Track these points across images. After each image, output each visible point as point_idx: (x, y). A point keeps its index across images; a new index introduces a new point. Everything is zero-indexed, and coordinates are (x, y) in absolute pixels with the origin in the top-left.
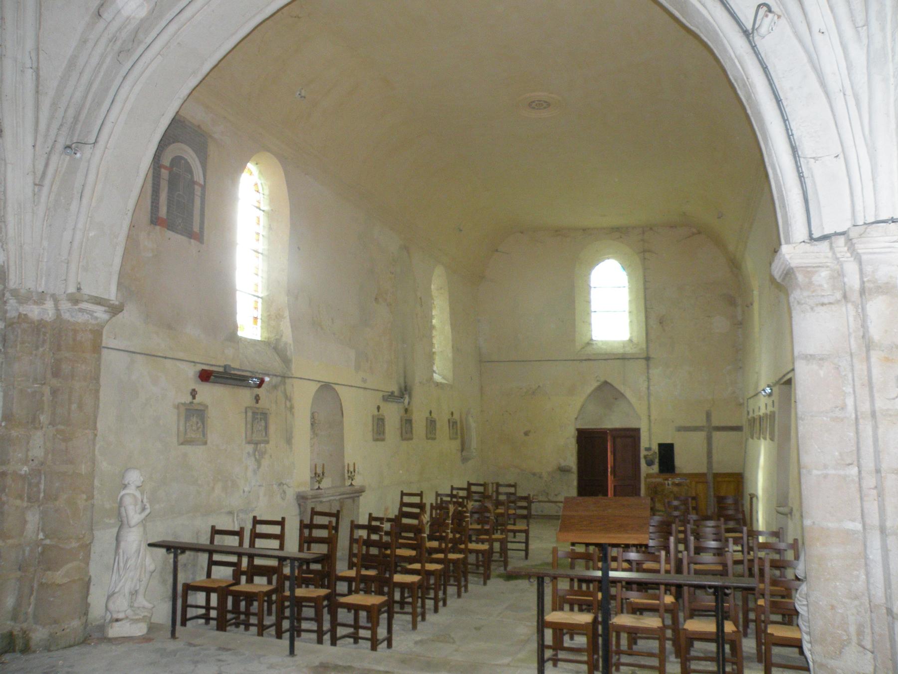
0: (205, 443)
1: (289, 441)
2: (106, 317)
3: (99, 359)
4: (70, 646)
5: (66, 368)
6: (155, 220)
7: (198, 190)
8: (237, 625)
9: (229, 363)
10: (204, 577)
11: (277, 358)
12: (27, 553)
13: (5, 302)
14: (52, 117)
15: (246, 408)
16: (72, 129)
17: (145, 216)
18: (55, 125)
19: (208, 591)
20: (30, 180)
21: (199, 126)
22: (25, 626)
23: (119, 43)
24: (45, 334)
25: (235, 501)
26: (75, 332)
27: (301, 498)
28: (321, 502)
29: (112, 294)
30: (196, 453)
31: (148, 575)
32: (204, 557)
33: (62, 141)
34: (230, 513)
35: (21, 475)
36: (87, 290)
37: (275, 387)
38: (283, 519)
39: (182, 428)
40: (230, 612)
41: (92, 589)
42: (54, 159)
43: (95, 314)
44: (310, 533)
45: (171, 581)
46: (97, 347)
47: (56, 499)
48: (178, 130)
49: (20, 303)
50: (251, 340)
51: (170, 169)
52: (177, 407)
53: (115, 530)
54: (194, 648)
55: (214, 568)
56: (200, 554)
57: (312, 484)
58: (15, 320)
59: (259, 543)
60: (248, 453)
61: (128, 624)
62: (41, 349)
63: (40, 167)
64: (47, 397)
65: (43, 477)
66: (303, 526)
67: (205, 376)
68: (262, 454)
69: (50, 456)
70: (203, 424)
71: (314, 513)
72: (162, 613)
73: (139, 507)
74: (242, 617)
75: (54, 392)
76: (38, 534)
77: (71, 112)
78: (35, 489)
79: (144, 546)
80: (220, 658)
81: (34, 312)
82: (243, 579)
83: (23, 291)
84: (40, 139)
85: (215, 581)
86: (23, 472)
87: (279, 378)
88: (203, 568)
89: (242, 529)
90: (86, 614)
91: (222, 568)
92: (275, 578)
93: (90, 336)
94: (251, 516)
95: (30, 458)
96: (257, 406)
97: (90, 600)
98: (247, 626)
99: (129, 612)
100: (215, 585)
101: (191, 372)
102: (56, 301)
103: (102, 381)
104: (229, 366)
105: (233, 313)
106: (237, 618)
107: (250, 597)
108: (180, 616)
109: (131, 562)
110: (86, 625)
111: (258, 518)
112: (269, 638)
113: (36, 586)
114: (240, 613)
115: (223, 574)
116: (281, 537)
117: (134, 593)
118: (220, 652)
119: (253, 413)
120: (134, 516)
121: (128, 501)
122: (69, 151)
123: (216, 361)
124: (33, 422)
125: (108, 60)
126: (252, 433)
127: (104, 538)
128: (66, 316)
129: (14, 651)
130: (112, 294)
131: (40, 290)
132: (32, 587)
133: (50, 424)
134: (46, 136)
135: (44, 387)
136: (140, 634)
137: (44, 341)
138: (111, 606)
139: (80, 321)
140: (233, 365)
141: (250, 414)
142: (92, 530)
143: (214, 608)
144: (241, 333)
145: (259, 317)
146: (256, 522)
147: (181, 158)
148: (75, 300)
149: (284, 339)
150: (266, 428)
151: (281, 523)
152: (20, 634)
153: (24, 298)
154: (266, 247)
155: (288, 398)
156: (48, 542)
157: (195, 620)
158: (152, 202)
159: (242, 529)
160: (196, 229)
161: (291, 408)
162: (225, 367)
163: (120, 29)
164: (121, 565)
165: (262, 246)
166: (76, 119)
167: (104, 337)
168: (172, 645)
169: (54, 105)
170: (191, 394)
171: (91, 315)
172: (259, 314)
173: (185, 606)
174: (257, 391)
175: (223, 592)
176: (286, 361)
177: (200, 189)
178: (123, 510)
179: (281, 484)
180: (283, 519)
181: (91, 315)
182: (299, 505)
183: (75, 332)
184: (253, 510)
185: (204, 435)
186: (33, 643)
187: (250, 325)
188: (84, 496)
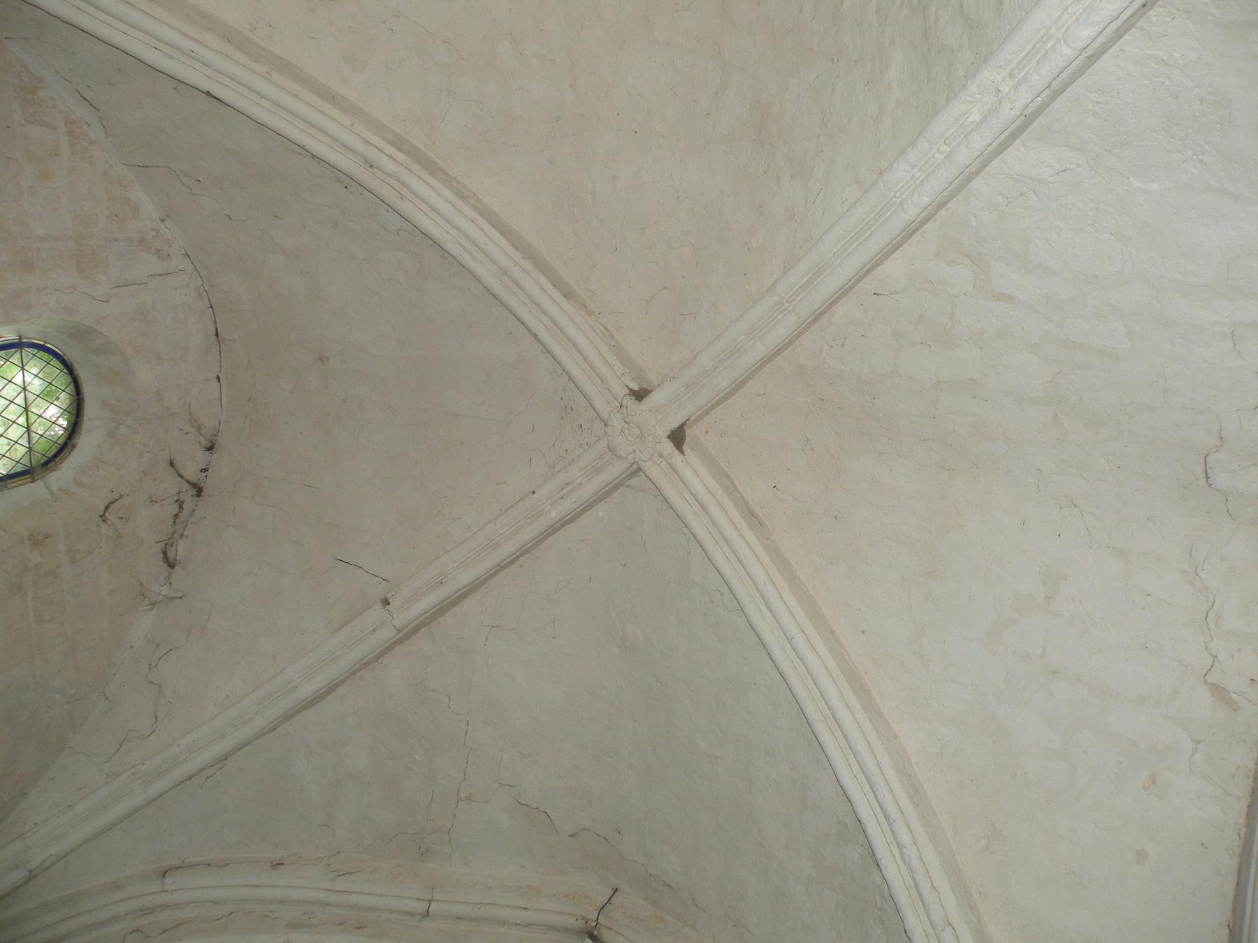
163: (165, 907)
182: (986, 60)
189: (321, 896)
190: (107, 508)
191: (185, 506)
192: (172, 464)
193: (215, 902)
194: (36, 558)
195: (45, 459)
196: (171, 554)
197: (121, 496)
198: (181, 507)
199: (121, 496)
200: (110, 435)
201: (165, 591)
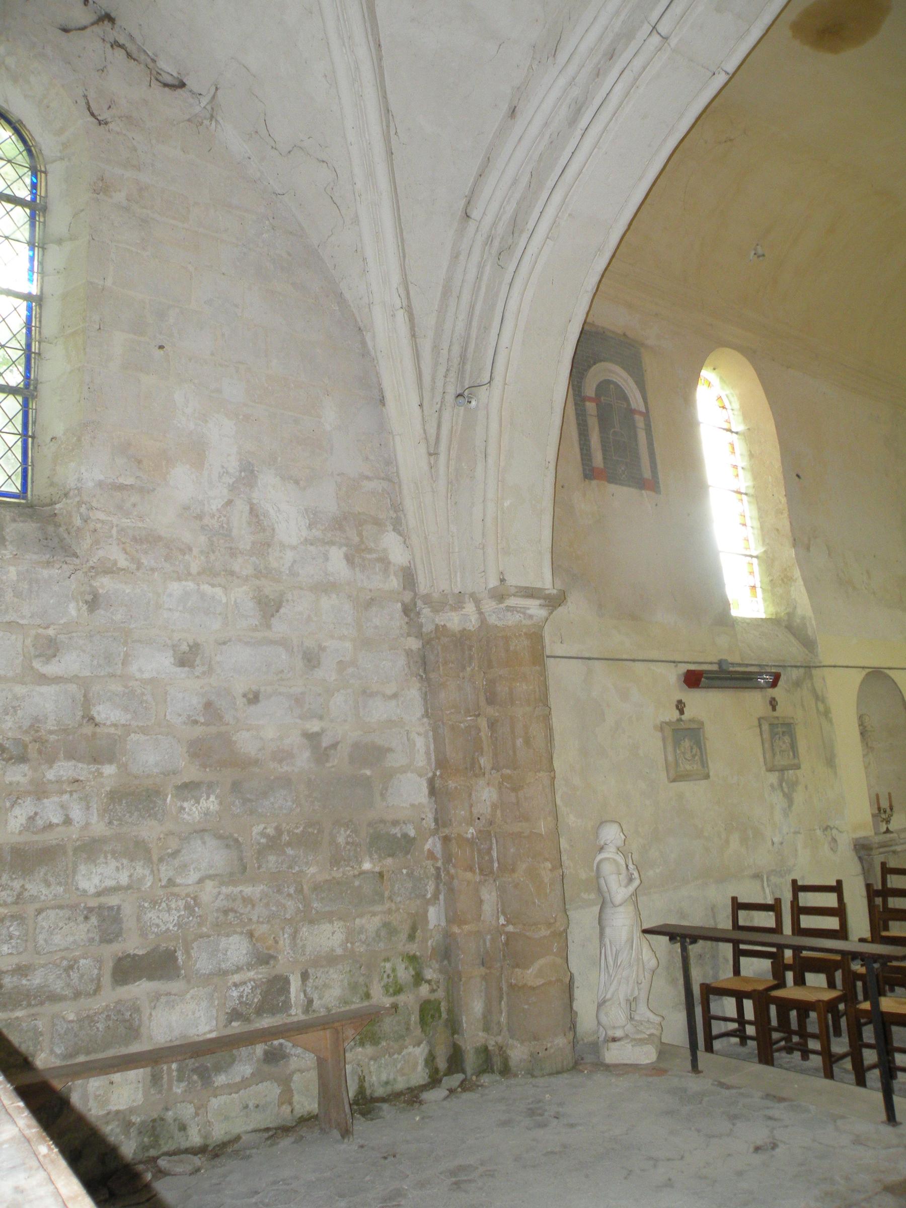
0: (707, 777)
1: (830, 761)
2: (543, 613)
3: (543, 673)
4: (558, 1073)
5: (502, 689)
6: (590, 473)
7: (640, 421)
8: (789, 1050)
9: (724, 657)
10: (730, 974)
11: (792, 639)
12: (488, 944)
13: (419, 613)
14: (436, 364)
15: (759, 719)
16: (461, 372)
17: (574, 469)
18: (442, 370)
19: (739, 995)
20: (423, 450)
21: (624, 335)
22: (500, 1039)
23: (496, 243)
24: (470, 649)
25: (762, 858)
26: (507, 639)
27: (862, 849)
28: (894, 852)
29: (546, 581)
30: (695, 793)
31: (648, 975)
32: (727, 949)
33: (452, 391)
34: (757, 876)
35: (468, 840)
36: (513, 581)
37: (798, 684)
38: (839, 882)
39: (671, 758)
40: (776, 1030)
41: (577, 993)
42: (446, 415)
43: (529, 612)
44: (885, 902)
45: (681, 981)
46: (538, 656)
47: (513, 871)
48: (592, 346)
49: (436, 611)
50: (751, 619)
51: (597, 399)
52: (661, 728)
53: (597, 909)
54: (727, 1093)
55: (743, 960)
56: (721, 944)
57: (876, 826)
58: (433, 635)
59: (807, 922)
60: (772, 786)
61: (629, 1046)
62: (468, 669)
63: (432, 431)
64: (485, 732)
65: (494, 841)
66: (871, 893)
67: (693, 680)
68: (793, 785)
69: (498, 812)
70: (700, 748)
71: (886, 870)
72: (676, 1029)
73: (623, 877)
74: (796, 1039)
75: (492, 725)
76: (498, 918)
77: (456, 349)
78: (487, 858)
79: (637, 933)
80: (770, 1113)
81: (453, 621)
82: (790, 976)
83: (436, 595)
84: (427, 395)
85: (747, 980)
86: (469, 836)
87: (802, 670)
88: (727, 960)
89: (778, 901)
90: (573, 1026)
91: (755, 960)
92: (838, 975)
93: (526, 643)
94: (789, 879)
95: (476, 816)
96: (775, 714)
97: (575, 1006)
98: (806, 1054)
99: (629, 1028)
100: (748, 988)
101: (672, 676)
102: (477, 602)
103: (552, 702)
104: (726, 661)
105: (719, 584)
106: (788, 1039)
107: (804, 1008)
108: (701, 1037)
109: (623, 957)
110: (574, 1043)
111: (800, 883)
112: (844, 1087)
113: (505, 988)
114: (791, 1033)
115: (756, 969)
116: (840, 912)
117: (631, 1002)
118: (768, 1103)
119: (772, 725)
120: (619, 892)
121: (607, 868)
122: (461, 399)
123: (708, 653)
124: (472, 769)
125: (488, 268)
126: (774, 755)
127: (582, 920)
128: (492, 620)
129: (493, 1072)
130: (546, 581)
131: (456, 591)
132: (501, 989)
133: (493, 768)
134: (433, 389)
135: (479, 719)
136: (648, 1061)
137: (471, 658)
138: (604, 1019)
139: (510, 623)
140: (730, 660)
141: (766, 727)
142: (565, 911)
143: (750, 1023)
144: (735, 612)
145: (758, 585)
146: (797, 888)
147: (608, 382)
148: (499, 596)
149: (799, 611)
150: (793, 746)
151: (837, 888)
152: (497, 1052)
153: (439, 605)
154: (750, 483)
155: (819, 698)
156: (510, 928)
157: (724, 1039)
158: (581, 449)
159: (778, 901)
160: (647, 474)
161: (827, 713)
162: (720, 663)
163: (494, 224)
164: (610, 960)
165: (745, 482)
166: (463, 359)
167: (547, 641)
168: (694, 1084)
169: (436, 348)
170: (677, 707)
171: (524, 614)
172: (757, 580)
173: (708, 1019)
174: (772, 692)
175: (762, 999)
176: (809, 644)
177: (642, 419)
178: (602, 881)
179: (827, 828)
180: (839, 882)
181: (524, 614)
182: (860, 858)
183: (507, 639)
184: (789, 871)
185: (704, 764)
186: (512, 1063)
187: (747, 595)
188: (549, 865)
189: (562, 81)
190: (92, 114)
191: (121, 42)
192: (66, 30)
193: (515, 182)
194: (120, 197)
195: (25, 153)
196: (169, 80)
197: (85, 96)
198: (121, 46)
199: (85, 96)
200: (15, 79)
201: (204, 101)
